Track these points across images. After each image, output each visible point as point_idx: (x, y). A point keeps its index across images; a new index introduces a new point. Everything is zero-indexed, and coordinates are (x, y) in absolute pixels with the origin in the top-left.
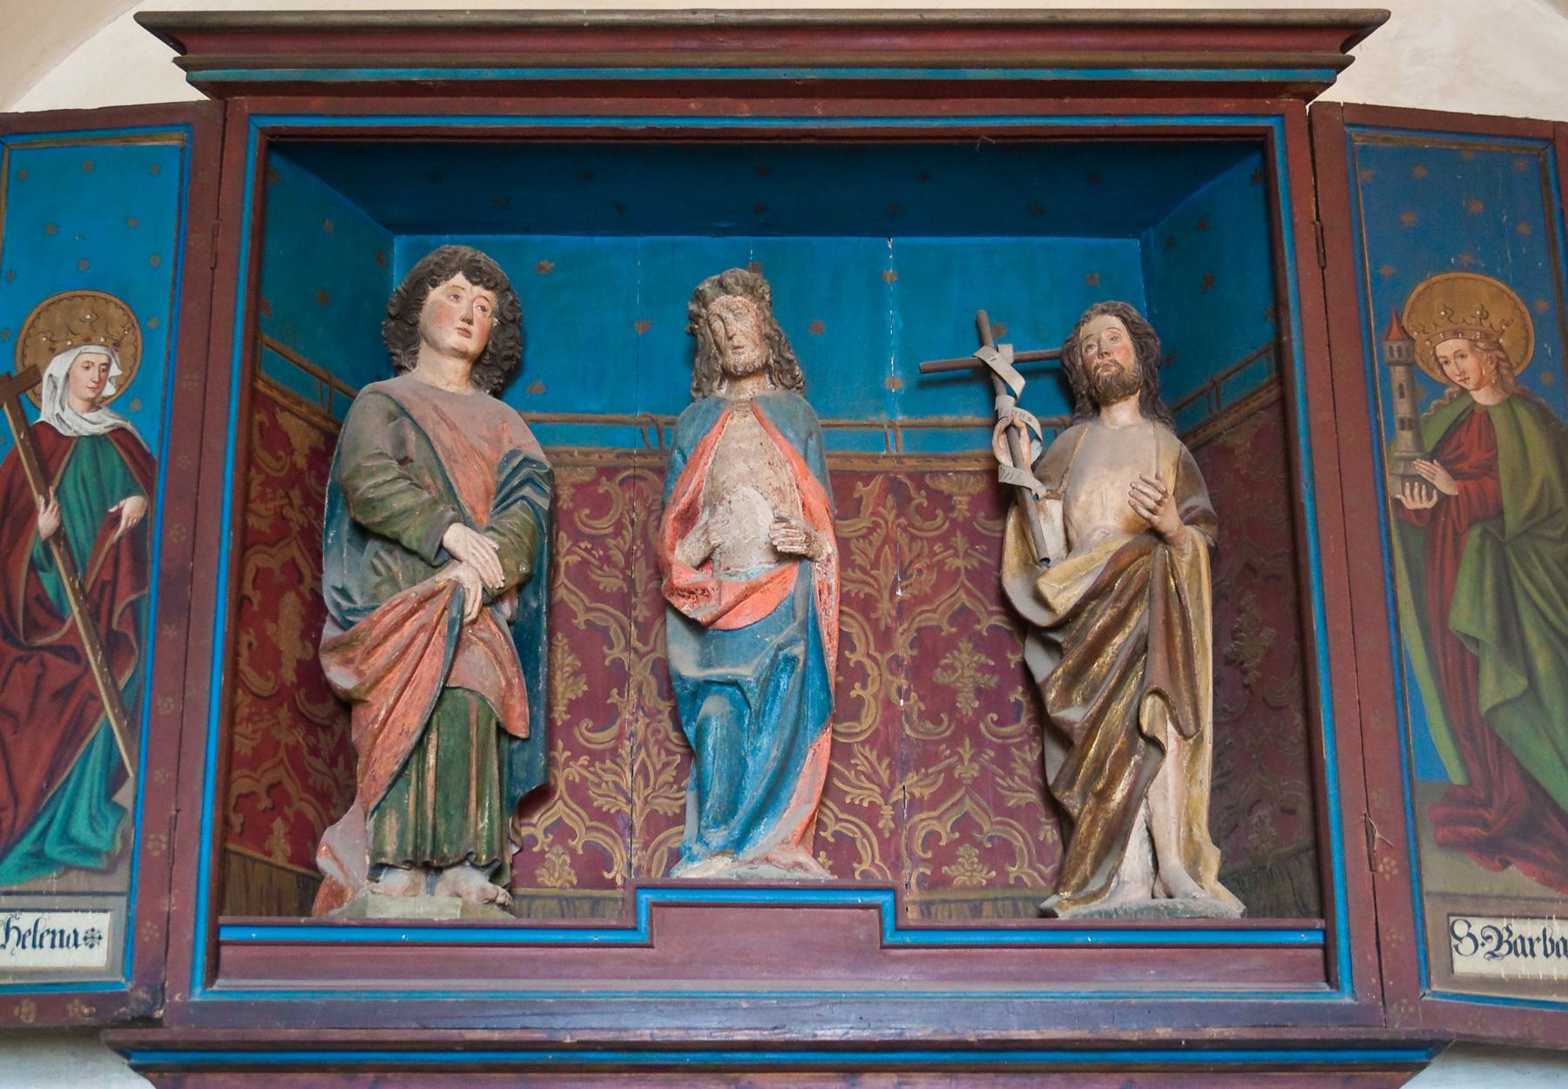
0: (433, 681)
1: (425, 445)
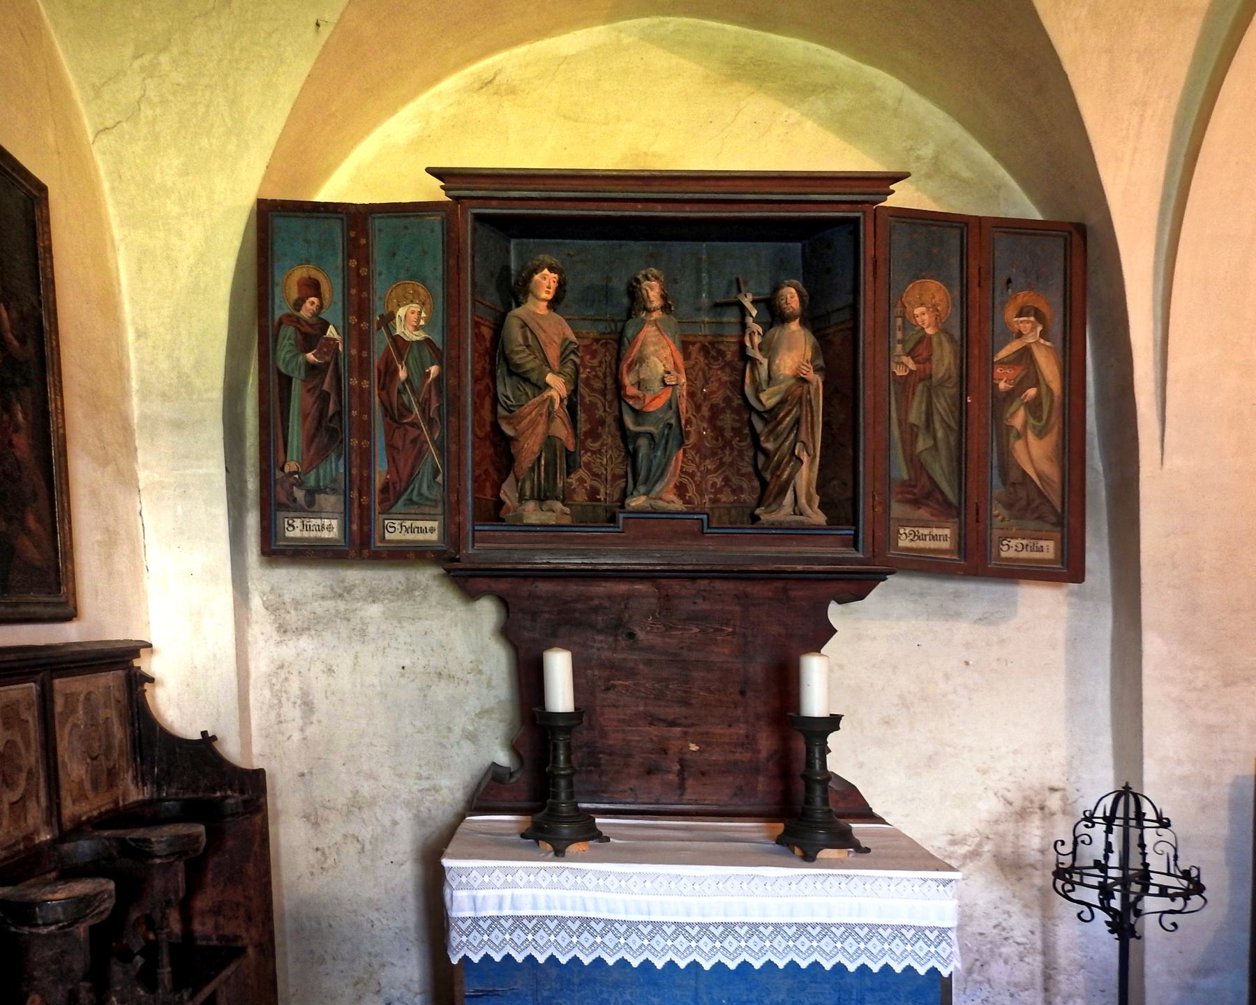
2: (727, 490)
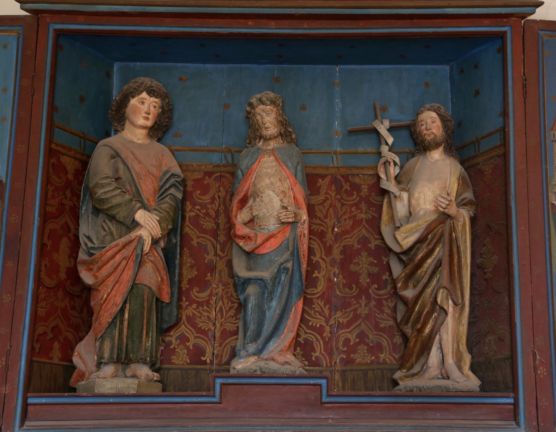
0: (128, 281)
1: (127, 171)
2: (363, 348)
